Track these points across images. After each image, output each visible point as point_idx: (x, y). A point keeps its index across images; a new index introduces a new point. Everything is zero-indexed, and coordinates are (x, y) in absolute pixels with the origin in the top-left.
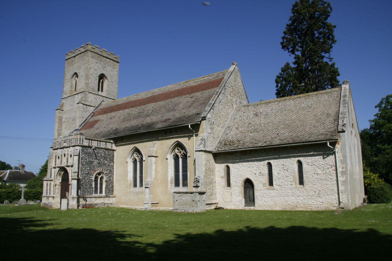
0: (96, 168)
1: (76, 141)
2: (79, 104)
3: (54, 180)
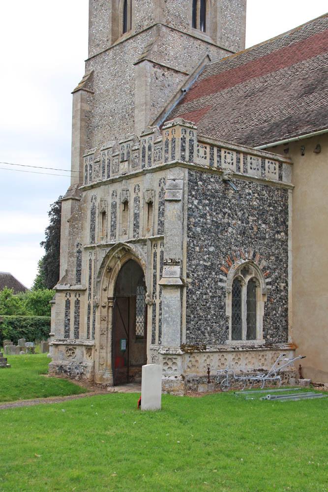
0: (234, 248)
1: (167, 151)
2: (141, 65)
3: (90, 289)
